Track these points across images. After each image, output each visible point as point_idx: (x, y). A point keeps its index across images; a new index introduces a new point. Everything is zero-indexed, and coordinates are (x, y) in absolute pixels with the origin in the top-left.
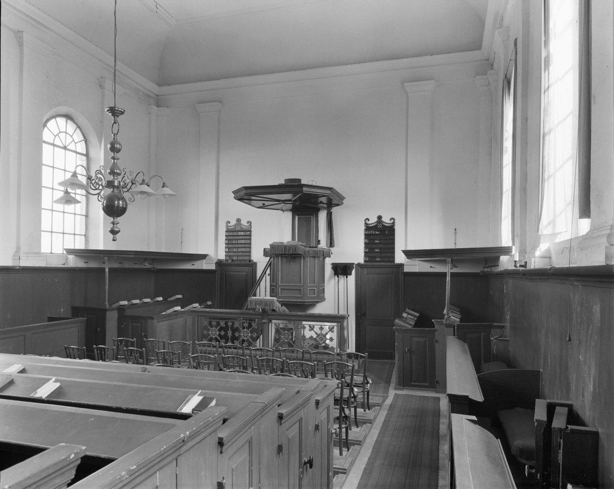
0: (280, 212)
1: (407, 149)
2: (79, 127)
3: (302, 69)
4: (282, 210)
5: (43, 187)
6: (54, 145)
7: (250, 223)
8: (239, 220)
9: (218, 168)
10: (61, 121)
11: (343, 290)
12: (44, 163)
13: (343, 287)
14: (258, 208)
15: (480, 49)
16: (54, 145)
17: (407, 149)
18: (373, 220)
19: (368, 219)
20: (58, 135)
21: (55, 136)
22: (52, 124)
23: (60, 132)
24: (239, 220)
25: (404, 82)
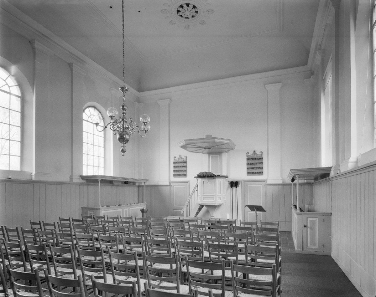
0: (202, 154)
1: (268, 125)
2: (100, 112)
3: (210, 80)
4: (203, 153)
5: (84, 120)
6: (88, 121)
7: (186, 157)
8: (180, 156)
9: (169, 127)
10: (91, 109)
11: (235, 207)
12: (83, 119)
13: (235, 206)
14: (191, 152)
15: (307, 65)
16: (88, 121)
17: (268, 125)
18: (251, 153)
19: (248, 153)
20: (90, 116)
21: (89, 117)
22: (87, 111)
23: (91, 115)
24: (180, 156)
25: (266, 84)
